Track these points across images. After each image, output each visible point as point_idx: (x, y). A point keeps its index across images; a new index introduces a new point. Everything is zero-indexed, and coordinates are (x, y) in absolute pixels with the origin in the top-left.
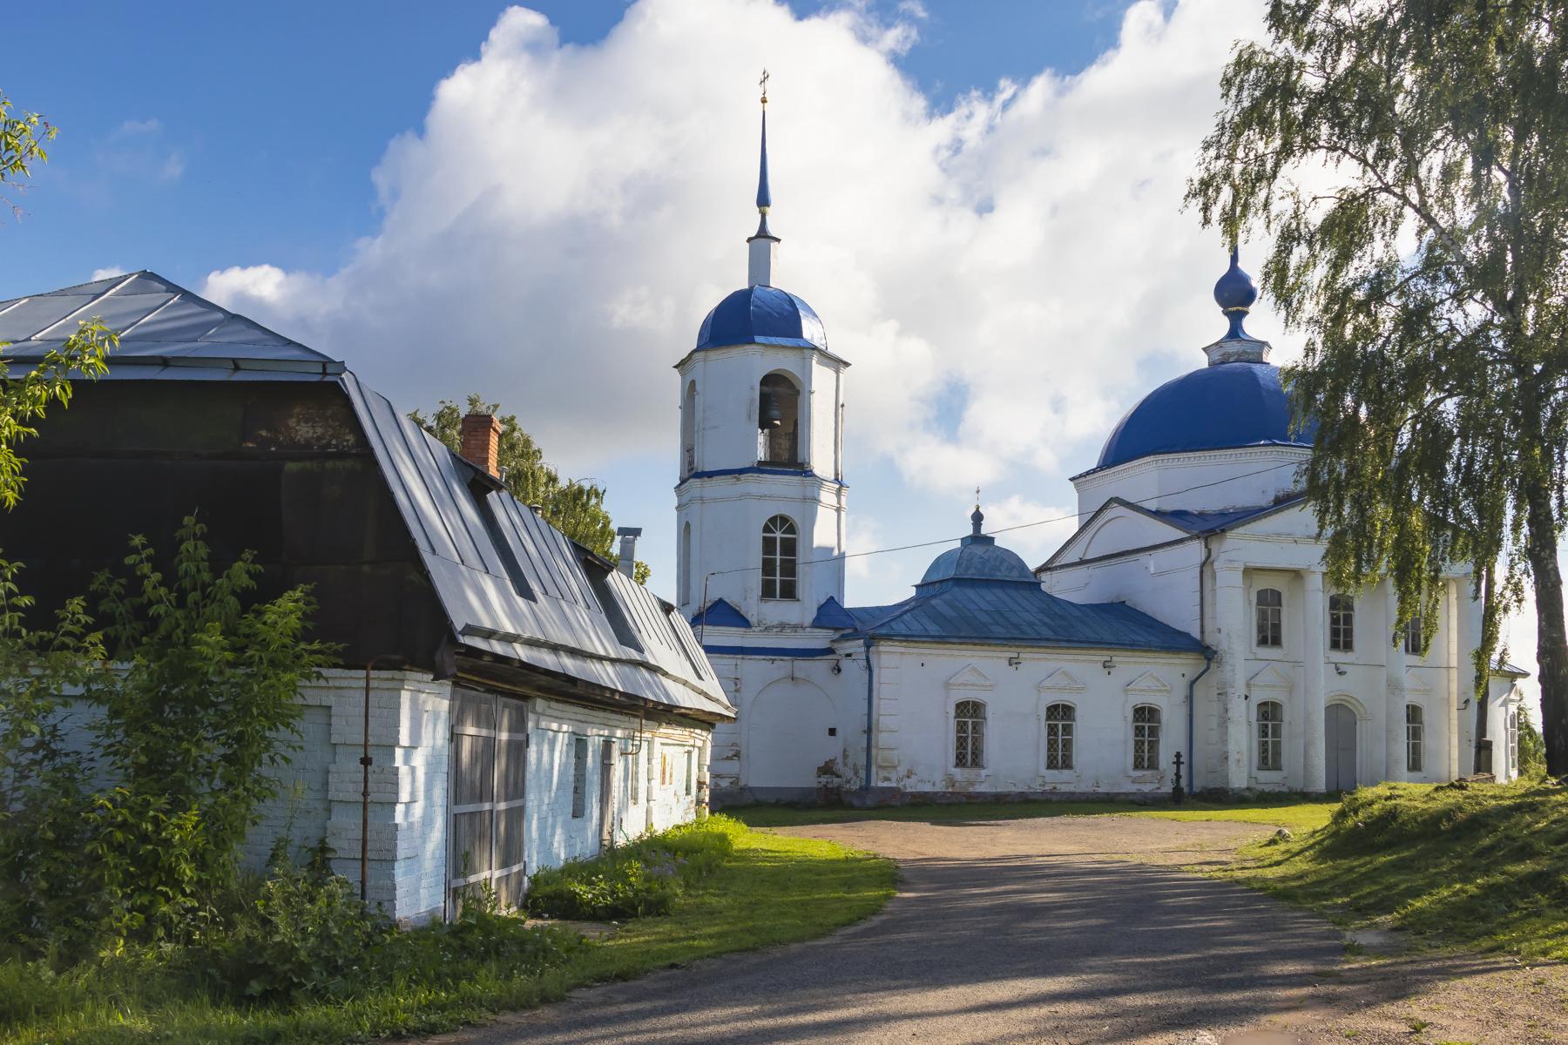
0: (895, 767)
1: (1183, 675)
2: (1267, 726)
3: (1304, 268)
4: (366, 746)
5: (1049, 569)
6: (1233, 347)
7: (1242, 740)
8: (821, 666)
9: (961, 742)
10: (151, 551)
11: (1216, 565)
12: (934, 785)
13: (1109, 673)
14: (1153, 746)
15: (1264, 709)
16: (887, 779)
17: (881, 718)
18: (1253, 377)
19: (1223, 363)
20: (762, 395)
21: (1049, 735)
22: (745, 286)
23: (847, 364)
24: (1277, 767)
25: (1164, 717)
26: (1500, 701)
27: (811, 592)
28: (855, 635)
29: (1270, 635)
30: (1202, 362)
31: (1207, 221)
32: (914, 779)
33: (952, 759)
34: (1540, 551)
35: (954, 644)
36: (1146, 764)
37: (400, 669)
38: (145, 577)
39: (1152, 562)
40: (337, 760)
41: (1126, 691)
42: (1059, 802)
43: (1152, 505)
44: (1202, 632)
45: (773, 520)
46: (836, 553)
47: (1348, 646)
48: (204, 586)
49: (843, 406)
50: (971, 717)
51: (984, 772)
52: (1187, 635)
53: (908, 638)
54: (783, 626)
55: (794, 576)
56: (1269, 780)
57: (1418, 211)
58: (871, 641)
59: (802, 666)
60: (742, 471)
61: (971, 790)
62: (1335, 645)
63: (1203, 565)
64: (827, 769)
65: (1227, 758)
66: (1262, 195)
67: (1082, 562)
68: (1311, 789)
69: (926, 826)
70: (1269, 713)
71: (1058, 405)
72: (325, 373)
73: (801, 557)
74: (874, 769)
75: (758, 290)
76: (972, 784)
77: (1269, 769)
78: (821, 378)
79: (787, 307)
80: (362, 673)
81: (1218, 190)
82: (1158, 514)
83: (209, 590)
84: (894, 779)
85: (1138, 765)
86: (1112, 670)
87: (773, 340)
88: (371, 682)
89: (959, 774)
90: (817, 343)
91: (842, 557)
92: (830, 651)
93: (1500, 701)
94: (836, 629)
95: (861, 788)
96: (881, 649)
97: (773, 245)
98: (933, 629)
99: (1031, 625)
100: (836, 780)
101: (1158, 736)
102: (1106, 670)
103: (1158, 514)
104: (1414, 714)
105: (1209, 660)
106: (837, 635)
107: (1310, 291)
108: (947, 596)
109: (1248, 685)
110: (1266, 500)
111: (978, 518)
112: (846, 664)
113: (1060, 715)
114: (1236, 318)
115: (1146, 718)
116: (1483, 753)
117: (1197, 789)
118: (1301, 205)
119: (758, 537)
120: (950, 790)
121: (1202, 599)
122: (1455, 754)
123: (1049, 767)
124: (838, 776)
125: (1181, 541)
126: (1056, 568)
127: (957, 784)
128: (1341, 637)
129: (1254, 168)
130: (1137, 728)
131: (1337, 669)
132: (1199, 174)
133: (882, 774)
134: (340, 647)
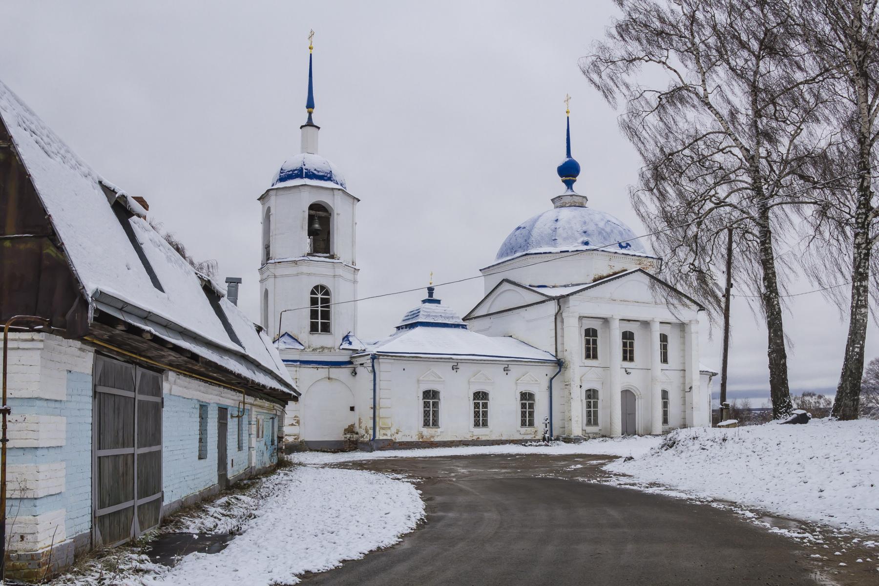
0: (390, 428)
1: (547, 375)
2: (590, 402)
11: (564, 315)
23: (359, 200)
24: (596, 423)
25: (537, 398)
41: (516, 383)
45: (316, 287)
47: (632, 359)
51: (439, 430)
61: (432, 440)
63: (556, 316)
65: (570, 420)
76: (433, 437)
84: (389, 435)
86: (508, 372)
89: (524, 430)
96: (380, 360)
101: (533, 409)
102: (506, 372)
120: (421, 440)
130: (522, 404)
131: (626, 371)
133: (382, 432)
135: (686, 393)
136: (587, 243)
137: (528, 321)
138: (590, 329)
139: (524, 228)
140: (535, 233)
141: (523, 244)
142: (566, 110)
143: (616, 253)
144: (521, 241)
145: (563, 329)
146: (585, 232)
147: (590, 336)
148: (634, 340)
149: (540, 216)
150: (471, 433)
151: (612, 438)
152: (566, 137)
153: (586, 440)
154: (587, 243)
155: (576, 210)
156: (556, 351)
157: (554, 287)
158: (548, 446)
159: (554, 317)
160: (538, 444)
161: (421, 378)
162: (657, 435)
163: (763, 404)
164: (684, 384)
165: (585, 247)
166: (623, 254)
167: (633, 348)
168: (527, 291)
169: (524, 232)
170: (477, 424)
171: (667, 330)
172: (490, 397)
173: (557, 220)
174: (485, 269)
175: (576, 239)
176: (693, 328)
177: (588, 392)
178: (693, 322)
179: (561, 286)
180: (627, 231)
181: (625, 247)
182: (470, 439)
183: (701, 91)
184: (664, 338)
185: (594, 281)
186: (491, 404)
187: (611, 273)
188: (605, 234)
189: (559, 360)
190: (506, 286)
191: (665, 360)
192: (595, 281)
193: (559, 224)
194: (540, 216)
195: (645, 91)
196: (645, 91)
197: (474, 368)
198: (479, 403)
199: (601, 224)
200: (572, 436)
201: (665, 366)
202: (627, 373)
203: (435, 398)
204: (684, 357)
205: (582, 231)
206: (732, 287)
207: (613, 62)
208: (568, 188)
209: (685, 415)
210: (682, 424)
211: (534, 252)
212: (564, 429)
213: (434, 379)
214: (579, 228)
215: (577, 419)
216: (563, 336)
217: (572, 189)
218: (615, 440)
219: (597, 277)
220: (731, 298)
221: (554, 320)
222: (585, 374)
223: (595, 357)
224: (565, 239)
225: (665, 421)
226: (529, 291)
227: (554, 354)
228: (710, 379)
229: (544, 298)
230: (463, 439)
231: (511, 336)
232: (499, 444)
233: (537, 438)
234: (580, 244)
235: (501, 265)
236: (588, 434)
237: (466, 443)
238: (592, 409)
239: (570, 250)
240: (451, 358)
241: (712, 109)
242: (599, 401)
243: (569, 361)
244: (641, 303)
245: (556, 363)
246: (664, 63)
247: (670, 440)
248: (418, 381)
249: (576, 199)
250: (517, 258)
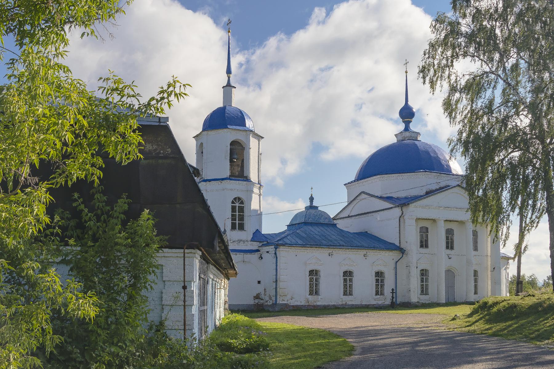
2: (423, 278)
3: (457, 101)
4: (184, 281)
5: (335, 219)
6: (407, 134)
7: (415, 283)
8: (256, 256)
9: (311, 286)
10: (82, 200)
12: (301, 302)
14: (382, 286)
15: (422, 272)
16: (283, 300)
17: (281, 276)
18: (416, 145)
19: (403, 140)
20: (230, 149)
21: (344, 282)
22: (221, 105)
23: (262, 138)
24: (427, 294)
26: (504, 268)
27: (250, 228)
28: (268, 244)
29: (424, 244)
30: (394, 140)
31: (424, 83)
32: (293, 300)
33: (308, 293)
34: (551, 209)
35: (308, 247)
36: (380, 294)
37: (194, 249)
38: (82, 210)
39: (378, 216)
40: (166, 288)
42: (349, 308)
43: (379, 194)
44: (400, 243)
45: (235, 199)
46: (259, 212)
47: (452, 248)
48: (107, 213)
49: (261, 154)
50: (315, 276)
51: (319, 297)
52: (394, 244)
53: (291, 245)
54: (240, 241)
55: (243, 221)
56: (425, 299)
57: (504, 81)
58: (277, 246)
59: (248, 256)
60: (223, 179)
61: (315, 304)
62: (447, 247)
64: (257, 297)
65: (410, 290)
66: (447, 73)
67: (349, 217)
68: (441, 302)
69: (305, 318)
70: (424, 273)
71: (284, 162)
72: (160, 122)
73: (246, 213)
74: (278, 297)
75: (228, 108)
77: (424, 295)
78: (253, 142)
79: (240, 114)
80: (182, 251)
81: (429, 70)
82: (381, 198)
83: (111, 213)
85: (377, 293)
87: (234, 127)
89: (311, 298)
90: (251, 129)
91: (261, 214)
92: (258, 251)
93: (504, 268)
94: (260, 242)
95: (273, 304)
97: (233, 89)
98: (300, 242)
99: (336, 240)
100: (261, 301)
103: (381, 198)
104: (476, 272)
105: (403, 253)
106: (261, 244)
107: (459, 111)
108: (302, 229)
109: (417, 263)
110: (423, 192)
111: (312, 199)
112: (265, 255)
113: (348, 274)
114: (407, 124)
115: (379, 275)
116: (519, 285)
117: (398, 303)
118: (458, 77)
119: (230, 205)
120: (307, 304)
121: (400, 230)
122: (490, 288)
123: (344, 295)
124: (262, 300)
125: (391, 208)
126: (338, 219)
128: (450, 245)
129: (444, 62)
132: (421, 64)
134: (167, 237)
186: (355, 279)
190: (363, 196)
198: (378, 279)
238: (424, 283)
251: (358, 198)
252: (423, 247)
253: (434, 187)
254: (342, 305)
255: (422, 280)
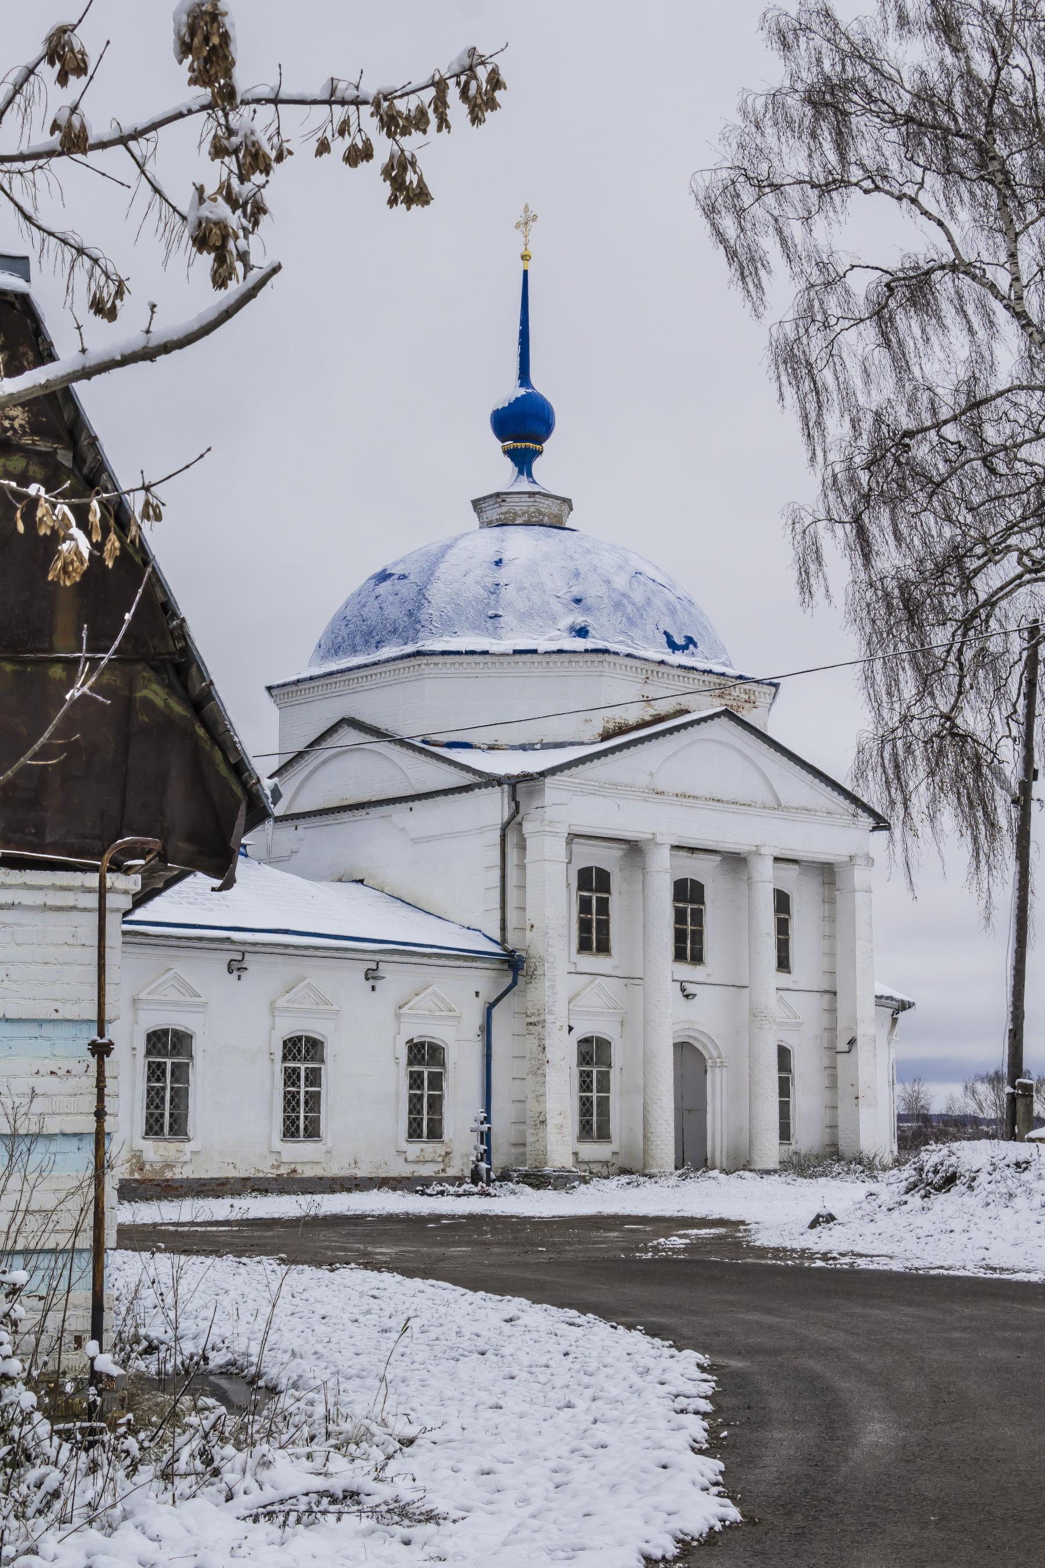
1: (477, 994)
2: (589, 1074)
11: (528, 828)
13: (373, 988)
24: (604, 1135)
25: (451, 1057)
41: (398, 1017)
47: (697, 958)
51: (188, 1147)
61: (168, 1175)
62: (680, 955)
65: (543, 1122)
76: (169, 1166)
80: (92, 880)
88: (96, 905)
89: (414, 1149)
101: (441, 1089)
102: (371, 982)
120: (137, 1176)
121: (503, 877)
127: (148, 1167)
131: (683, 990)
135: (840, 1057)
136: (582, 632)
137: (415, 841)
138: (590, 869)
139: (403, 577)
140: (438, 593)
141: (403, 621)
142: (521, 250)
143: (662, 662)
144: (395, 613)
145: (522, 867)
146: (578, 601)
147: (590, 890)
148: (703, 903)
149: (449, 547)
150: (274, 1157)
151: (651, 1177)
152: (517, 328)
153: (585, 1181)
154: (582, 632)
155: (549, 536)
156: (503, 929)
157: (491, 748)
158: (488, 1195)
159: (498, 833)
160: (461, 1190)
161: (143, 996)
162: (768, 1172)
163: (952, 1099)
164: (832, 1029)
165: (580, 644)
166: (680, 666)
167: (701, 925)
168: (417, 755)
169: (406, 590)
170: (290, 1131)
171: (790, 880)
172: (328, 1052)
173: (498, 563)
174: (284, 685)
175: (554, 620)
176: (860, 876)
177: (585, 1045)
178: (858, 861)
179: (513, 748)
180: (686, 603)
181: (685, 648)
182: (272, 1173)
183: (1003, 279)
184: (782, 902)
185: (606, 736)
186: (329, 1072)
187: (648, 718)
188: (629, 608)
189: (511, 953)
190: (349, 737)
191: (783, 964)
192: (606, 736)
193: (503, 575)
194: (449, 547)
195: (853, 267)
196: (853, 267)
197: (286, 969)
199: (620, 582)
200: (548, 1169)
201: (784, 979)
202: (687, 996)
203: (179, 1054)
204: (831, 954)
205: (568, 597)
206: (1035, 778)
207: (776, 187)
208: (521, 472)
209: (835, 1117)
210: (827, 1141)
211: (439, 647)
212: (520, 1150)
213: (177, 997)
214: (559, 586)
215: (559, 1120)
216: (522, 887)
217: (530, 475)
218: (662, 1181)
219: (611, 726)
220: (1034, 807)
221: (498, 840)
222: (578, 994)
223: (604, 948)
224: (525, 617)
225: (785, 1134)
226: (422, 757)
227: (497, 936)
228: (895, 1021)
229: (468, 779)
230: (250, 1173)
231: (361, 881)
232: (349, 1190)
233: (451, 1172)
234: (565, 634)
235: (338, 678)
236: (587, 1163)
237: (260, 1186)
239: (541, 649)
240: (228, 939)
241: (1031, 329)
242: (612, 1072)
243: (541, 958)
244: (728, 802)
245: (503, 962)
246: (914, 201)
247: (936, 1172)
248: (135, 1001)
249: (544, 505)
250: (388, 661)
251: (329, 742)
252: (589, 948)
253: (633, 714)
254: (276, 1179)
255: (584, 1082)
